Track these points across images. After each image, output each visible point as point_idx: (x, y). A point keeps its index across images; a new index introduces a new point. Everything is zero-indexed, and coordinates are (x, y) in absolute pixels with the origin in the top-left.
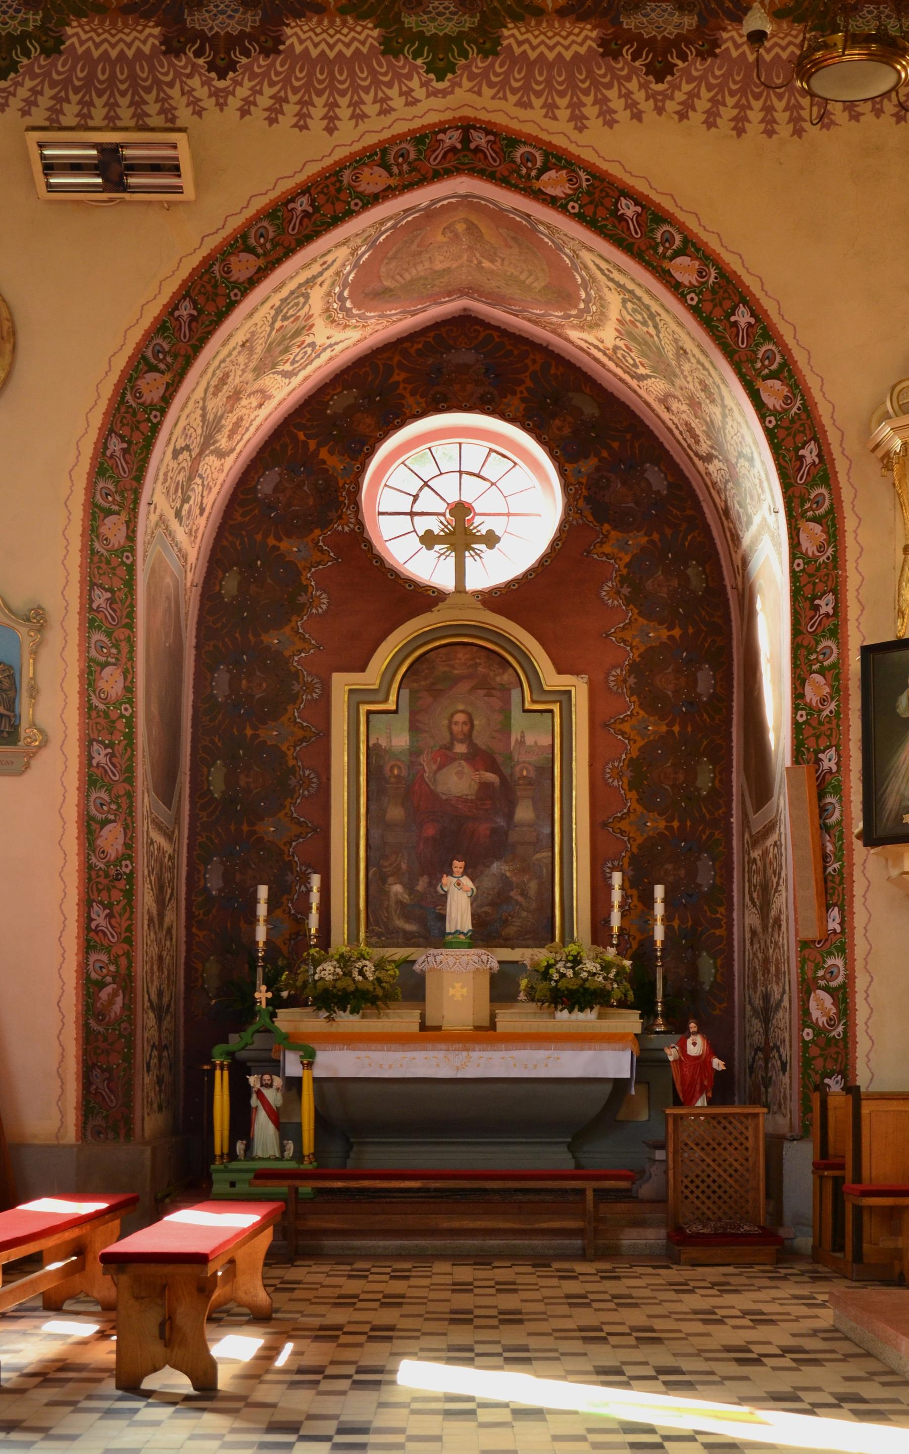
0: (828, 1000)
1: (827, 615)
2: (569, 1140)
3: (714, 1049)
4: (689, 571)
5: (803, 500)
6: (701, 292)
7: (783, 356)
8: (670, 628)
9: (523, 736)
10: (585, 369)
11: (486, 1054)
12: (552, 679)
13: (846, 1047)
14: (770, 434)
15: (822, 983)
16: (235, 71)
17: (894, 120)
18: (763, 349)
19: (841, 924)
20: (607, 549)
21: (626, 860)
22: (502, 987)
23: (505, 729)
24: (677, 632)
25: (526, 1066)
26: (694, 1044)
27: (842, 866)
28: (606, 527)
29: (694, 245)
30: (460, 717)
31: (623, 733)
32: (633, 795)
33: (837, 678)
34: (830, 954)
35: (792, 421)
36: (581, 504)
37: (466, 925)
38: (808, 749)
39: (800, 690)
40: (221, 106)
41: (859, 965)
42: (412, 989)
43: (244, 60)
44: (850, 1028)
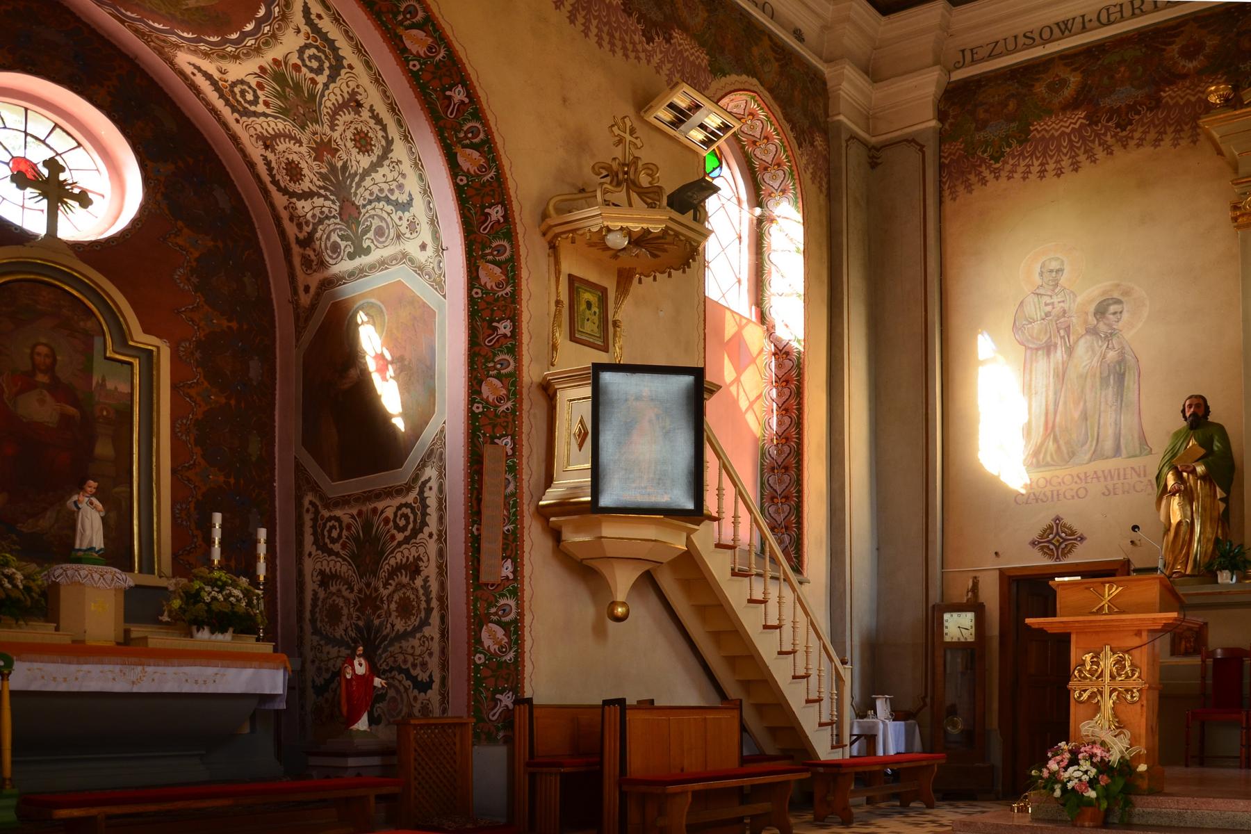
0: (500, 633)
1: (505, 336)
3: (374, 670)
4: (245, 279)
5: (484, 247)
6: (425, 63)
7: (487, 135)
8: (229, 321)
9: (104, 380)
10: (166, 90)
11: (160, 669)
12: (141, 338)
13: (516, 669)
14: (459, 191)
15: (494, 618)
18: (470, 124)
19: (514, 572)
20: (180, 240)
21: (192, 505)
22: (140, 605)
23: (87, 372)
24: (234, 325)
25: (196, 682)
26: (360, 665)
27: (515, 528)
28: (180, 223)
29: (433, 25)
30: (42, 349)
31: (191, 397)
32: (197, 450)
33: (514, 384)
34: (503, 596)
35: (483, 185)
36: (159, 197)
37: (99, 543)
38: (484, 435)
39: (476, 387)
41: (526, 605)
42: (44, 605)
43: (1137, 117)
44: (519, 655)
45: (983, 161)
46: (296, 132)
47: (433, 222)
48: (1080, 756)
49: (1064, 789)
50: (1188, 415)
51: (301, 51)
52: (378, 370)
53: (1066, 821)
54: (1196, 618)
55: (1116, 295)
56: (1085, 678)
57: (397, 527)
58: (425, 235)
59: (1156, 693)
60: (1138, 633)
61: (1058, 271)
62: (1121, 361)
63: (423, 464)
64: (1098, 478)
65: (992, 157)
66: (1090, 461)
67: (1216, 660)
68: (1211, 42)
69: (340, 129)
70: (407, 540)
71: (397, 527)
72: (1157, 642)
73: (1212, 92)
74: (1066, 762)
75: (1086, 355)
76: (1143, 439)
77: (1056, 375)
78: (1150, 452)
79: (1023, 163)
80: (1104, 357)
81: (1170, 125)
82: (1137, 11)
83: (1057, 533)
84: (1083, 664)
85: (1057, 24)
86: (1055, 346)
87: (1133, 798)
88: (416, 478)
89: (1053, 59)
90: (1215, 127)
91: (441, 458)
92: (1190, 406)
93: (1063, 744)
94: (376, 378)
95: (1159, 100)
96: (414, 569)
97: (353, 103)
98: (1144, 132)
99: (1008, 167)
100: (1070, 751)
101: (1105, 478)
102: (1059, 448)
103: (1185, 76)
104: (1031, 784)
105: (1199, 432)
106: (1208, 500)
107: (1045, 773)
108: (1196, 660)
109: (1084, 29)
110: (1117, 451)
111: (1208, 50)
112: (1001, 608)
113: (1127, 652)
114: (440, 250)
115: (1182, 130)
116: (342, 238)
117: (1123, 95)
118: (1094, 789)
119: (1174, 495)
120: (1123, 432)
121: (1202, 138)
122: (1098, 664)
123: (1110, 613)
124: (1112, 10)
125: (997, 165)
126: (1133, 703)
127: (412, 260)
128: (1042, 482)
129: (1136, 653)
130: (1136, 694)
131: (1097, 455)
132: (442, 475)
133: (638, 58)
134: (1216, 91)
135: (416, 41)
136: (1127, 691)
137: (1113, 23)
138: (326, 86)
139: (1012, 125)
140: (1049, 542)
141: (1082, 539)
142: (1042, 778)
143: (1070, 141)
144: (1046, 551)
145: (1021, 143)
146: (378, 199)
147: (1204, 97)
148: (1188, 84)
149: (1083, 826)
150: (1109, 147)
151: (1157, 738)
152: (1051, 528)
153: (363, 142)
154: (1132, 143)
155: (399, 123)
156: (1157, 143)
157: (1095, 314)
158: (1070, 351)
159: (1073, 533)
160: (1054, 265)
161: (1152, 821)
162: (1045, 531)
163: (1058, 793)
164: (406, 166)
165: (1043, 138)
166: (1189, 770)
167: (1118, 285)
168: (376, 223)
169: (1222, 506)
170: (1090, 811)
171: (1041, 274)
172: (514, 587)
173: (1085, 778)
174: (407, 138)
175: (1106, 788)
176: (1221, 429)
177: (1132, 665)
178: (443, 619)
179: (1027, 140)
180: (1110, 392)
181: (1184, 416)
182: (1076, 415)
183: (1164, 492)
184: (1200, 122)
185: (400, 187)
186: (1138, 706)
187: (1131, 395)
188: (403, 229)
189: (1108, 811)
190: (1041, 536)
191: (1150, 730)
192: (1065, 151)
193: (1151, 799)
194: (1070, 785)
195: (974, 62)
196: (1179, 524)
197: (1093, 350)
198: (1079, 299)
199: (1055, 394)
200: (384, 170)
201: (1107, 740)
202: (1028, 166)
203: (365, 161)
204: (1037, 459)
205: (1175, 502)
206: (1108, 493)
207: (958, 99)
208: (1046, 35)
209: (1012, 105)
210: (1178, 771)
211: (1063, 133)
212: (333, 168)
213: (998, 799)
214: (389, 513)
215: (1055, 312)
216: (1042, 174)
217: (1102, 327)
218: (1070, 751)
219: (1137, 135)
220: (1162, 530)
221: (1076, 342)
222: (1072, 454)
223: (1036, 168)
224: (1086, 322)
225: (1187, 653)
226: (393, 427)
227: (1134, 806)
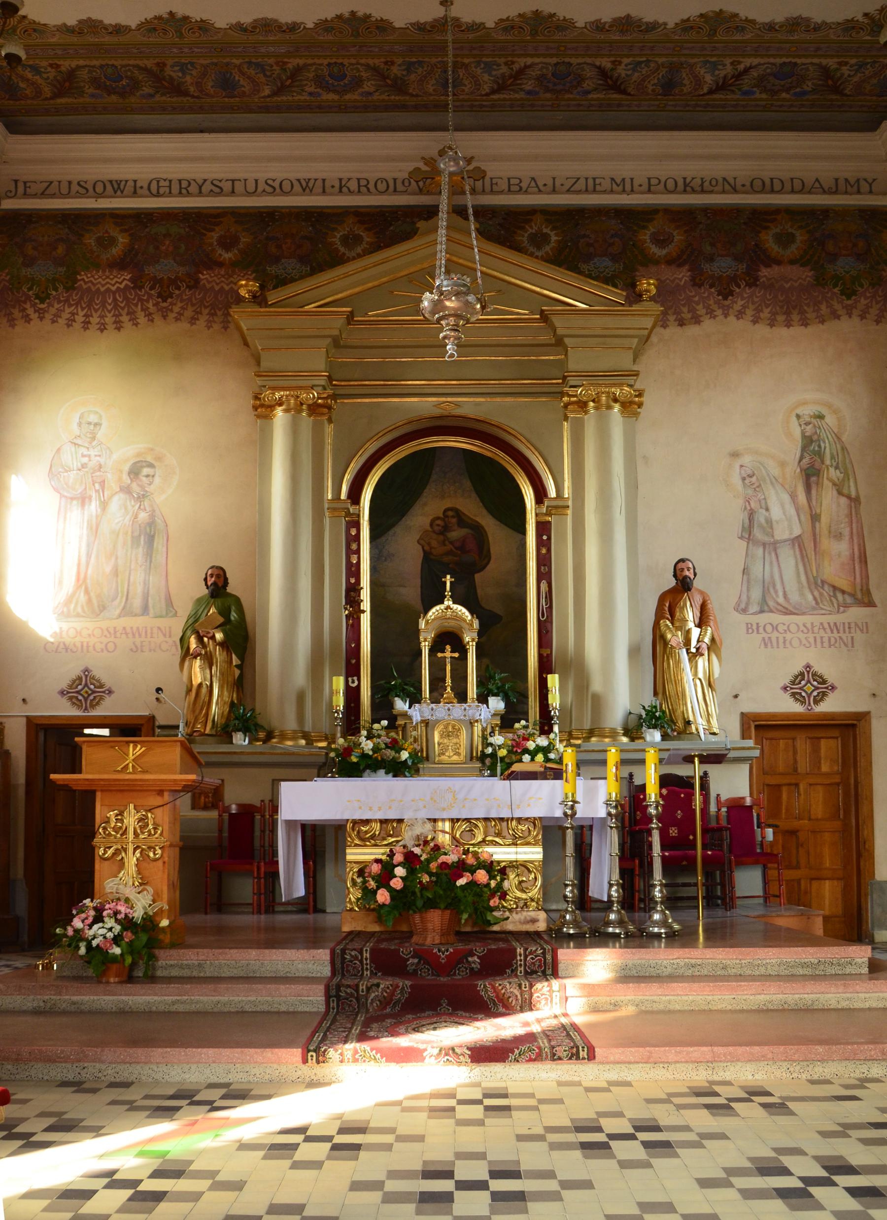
2: (676, 927)
16: (172, 297)
17: (859, 318)
40: (41, 319)
43: (177, 292)
45: (28, 298)
48: (105, 913)
49: (89, 947)
50: (209, 583)
53: (92, 978)
54: (212, 778)
55: (149, 459)
56: (110, 835)
59: (177, 850)
60: (160, 793)
61: (96, 425)
62: (152, 523)
64: (127, 634)
65: (37, 297)
66: (119, 616)
67: (231, 815)
68: (245, 239)
72: (178, 802)
73: (242, 286)
74: (91, 919)
75: (120, 513)
77: (90, 527)
78: (175, 615)
79: (68, 310)
80: (136, 517)
81: (206, 307)
82: (184, 191)
83: (86, 685)
84: (108, 821)
85: (111, 182)
86: (90, 498)
87: (156, 952)
89: (105, 214)
90: (245, 318)
92: (212, 576)
93: (87, 901)
95: (197, 281)
98: (182, 308)
99: (53, 310)
100: (95, 908)
101: (134, 635)
102: (90, 601)
103: (221, 265)
104: (54, 942)
105: (219, 601)
106: (225, 665)
107: (70, 931)
108: (214, 814)
109: (135, 194)
110: (145, 610)
111: (241, 246)
112: (27, 753)
113: (150, 811)
115: (215, 314)
117: (166, 268)
118: (118, 946)
119: (195, 657)
120: (151, 592)
121: (232, 326)
122: (122, 821)
123: (134, 772)
124: (162, 183)
125: (42, 306)
126: (156, 860)
128: (72, 633)
129: (158, 811)
130: (159, 851)
131: (126, 611)
134: (246, 285)
136: (150, 848)
137: (162, 196)
139: (60, 269)
140: (77, 692)
141: (110, 692)
142: (66, 936)
143: (115, 299)
144: (75, 701)
145: (67, 289)
147: (236, 288)
148: (222, 273)
149: (108, 982)
150: (150, 314)
151: (178, 893)
152: (80, 679)
154: (172, 316)
156: (193, 321)
157: (129, 474)
158: (104, 505)
159: (101, 686)
160: (93, 418)
161: (175, 973)
162: (74, 681)
163: (83, 951)
165: (89, 289)
166: (208, 917)
167: (152, 450)
169: (237, 672)
170: (114, 967)
171: (80, 424)
173: (110, 935)
175: (131, 944)
176: (237, 601)
177: (154, 824)
179: (73, 288)
181: (206, 584)
182: (108, 569)
183: (186, 654)
184: (231, 311)
186: (160, 863)
187: (159, 558)
189: (134, 965)
190: (71, 687)
191: (171, 886)
192: (109, 308)
193: (173, 952)
194: (94, 943)
195: (25, 195)
196: (200, 685)
197: (126, 508)
198: (115, 457)
199: (88, 546)
201: (131, 897)
202: (73, 314)
204: (64, 615)
206: (136, 649)
208: (99, 189)
209: (61, 250)
210: (199, 919)
211: (108, 290)
213: (23, 950)
215: (91, 464)
216: (86, 325)
217: (134, 486)
218: (95, 908)
219: (176, 309)
220: (185, 689)
221: (110, 498)
222: (103, 608)
223: (80, 318)
224: (120, 479)
225: (205, 808)
227: (157, 960)
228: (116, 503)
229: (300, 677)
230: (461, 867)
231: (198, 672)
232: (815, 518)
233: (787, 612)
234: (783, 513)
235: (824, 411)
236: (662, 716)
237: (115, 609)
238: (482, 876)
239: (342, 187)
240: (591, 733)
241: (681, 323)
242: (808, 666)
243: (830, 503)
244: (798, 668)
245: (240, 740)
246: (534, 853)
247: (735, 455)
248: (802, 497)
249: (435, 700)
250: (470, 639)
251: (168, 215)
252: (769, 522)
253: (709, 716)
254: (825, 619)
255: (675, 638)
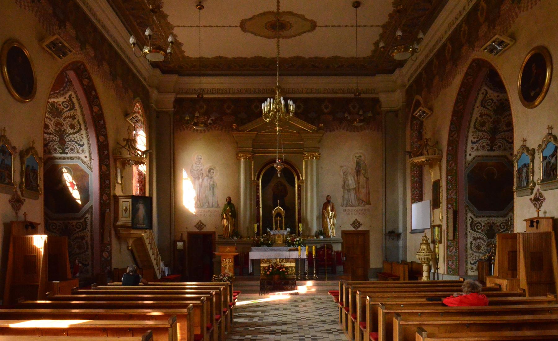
44: (111, 258)
46: (51, 118)
47: (90, 152)
51: (63, 102)
52: (71, 186)
57: (77, 227)
58: (87, 154)
62: (213, 185)
63: (86, 213)
69: (66, 121)
70: (80, 231)
71: (77, 227)
76: (218, 204)
88: (83, 216)
91: (92, 212)
94: (70, 189)
96: (83, 238)
97: (73, 117)
110: (213, 206)
114: (91, 159)
116: (58, 147)
127: (82, 160)
132: (92, 216)
133: (25, 9)
135: (96, 109)
138: (67, 111)
144: (198, 228)
146: (73, 141)
153: (72, 126)
155: (85, 126)
156: (221, 130)
158: (203, 180)
160: (200, 157)
164: (84, 136)
168: (71, 147)
172: (110, 244)
174: (86, 129)
178: (92, 250)
180: (211, 191)
182: (204, 196)
185: (81, 140)
188: (80, 151)
200: (77, 135)
203: (71, 131)
205: (225, 221)
207: (178, 102)
212: (60, 130)
214: (74, 224)
217: (210, 175)
226: (77, 203)
228: (206, 179)
229: (247, 224)
230: (281, 268)
231: (225, 223)
232: (359, 183)
233: (352, 206)
234: (351, 181)
235: (361, 155)
236: (323, 232)
237: (206, 206)
238: (284, 269)
239: (255, 92)
240: (308, 236)
241: (330, 131)
242: (356, 220)
243: (362, 179)
244: (354, 219)
245: (235, 238)
246: (293, 265)
247: (341, 167)
248: (356, 178)
249: (276, 229)
250: (283, 215)
251: (215, 99)
252: (349, 184)
253: (333, 232)
254: (360, 208)
255: (326, 215)
